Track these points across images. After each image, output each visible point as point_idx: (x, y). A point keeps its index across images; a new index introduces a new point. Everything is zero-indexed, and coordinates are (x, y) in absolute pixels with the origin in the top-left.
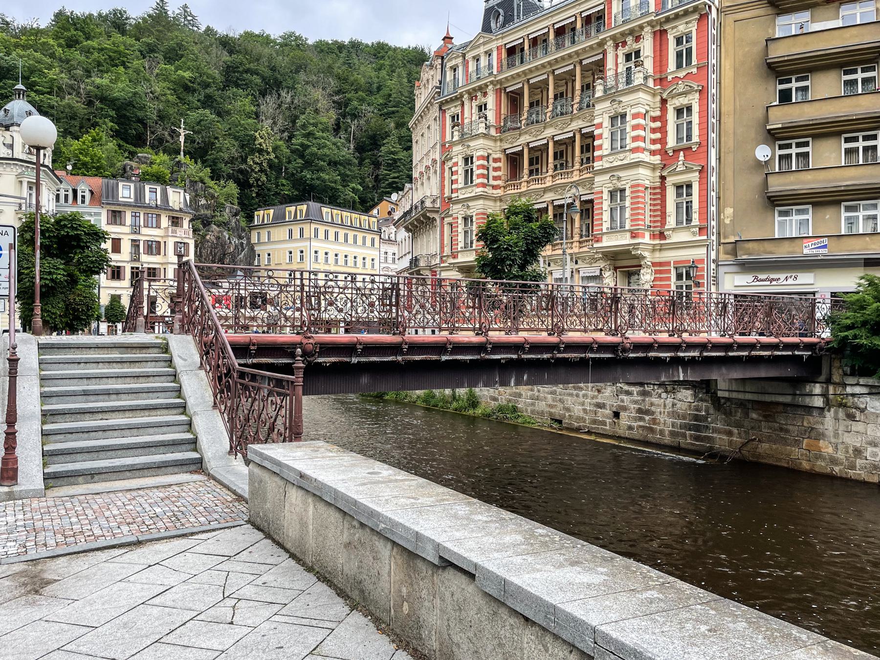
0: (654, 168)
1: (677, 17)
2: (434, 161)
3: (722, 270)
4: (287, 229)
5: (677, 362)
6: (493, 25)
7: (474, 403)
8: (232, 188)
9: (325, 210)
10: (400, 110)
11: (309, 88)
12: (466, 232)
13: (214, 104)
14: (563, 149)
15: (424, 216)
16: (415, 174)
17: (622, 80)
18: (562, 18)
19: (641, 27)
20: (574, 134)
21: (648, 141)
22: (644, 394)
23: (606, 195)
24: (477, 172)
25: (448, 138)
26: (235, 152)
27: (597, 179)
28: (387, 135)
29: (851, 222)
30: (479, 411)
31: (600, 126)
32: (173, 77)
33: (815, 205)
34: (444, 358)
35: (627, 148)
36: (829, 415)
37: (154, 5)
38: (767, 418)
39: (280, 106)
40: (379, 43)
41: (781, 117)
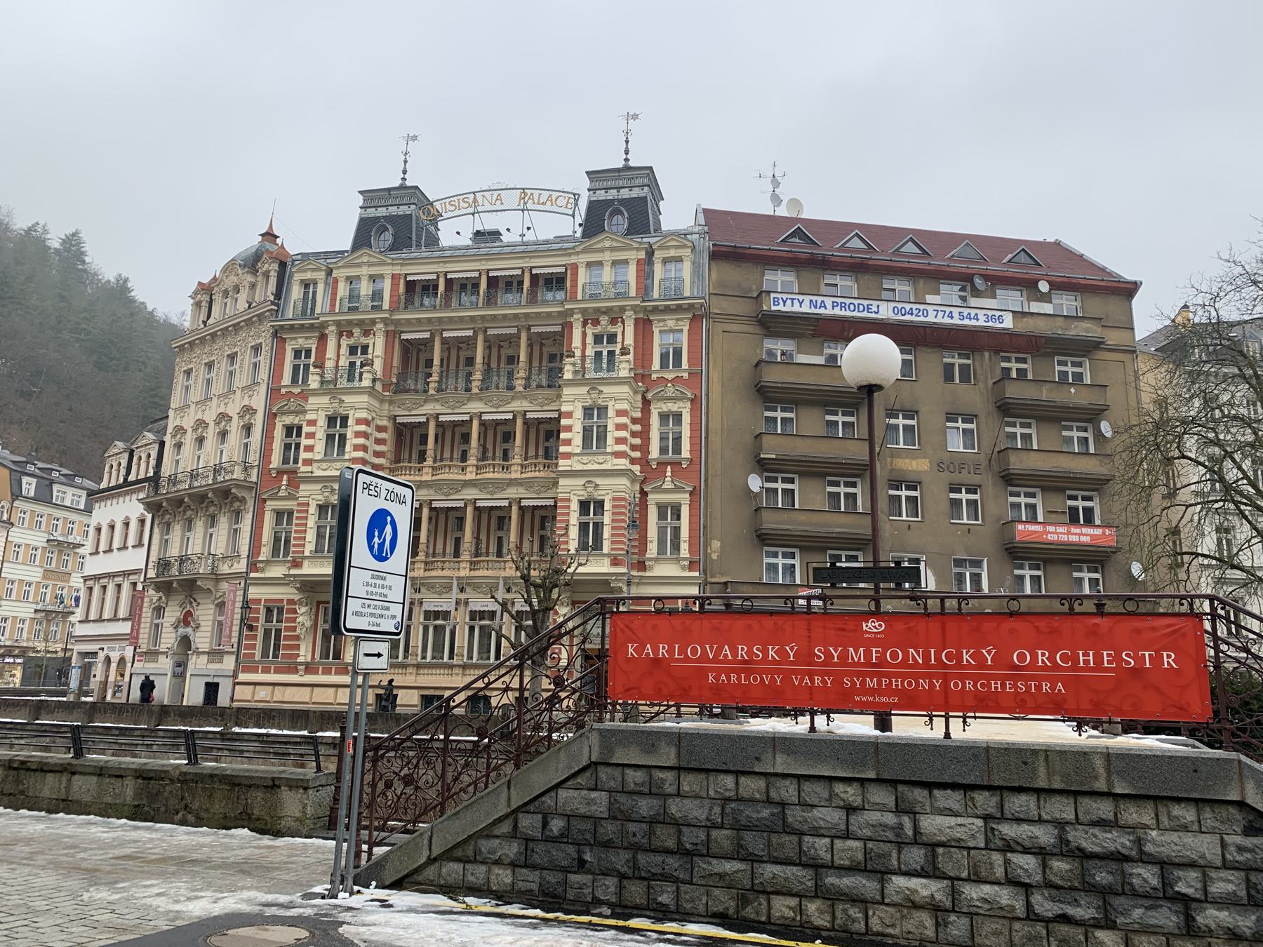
1: (667, 310)
14: (498, 434)
18: (460, 270)
19: (373, 322)
20: (515, 417)
21: (370, 451)
23: (575, 506)
24: (351, 441)
27: (562, 482)
35: (347, 457)
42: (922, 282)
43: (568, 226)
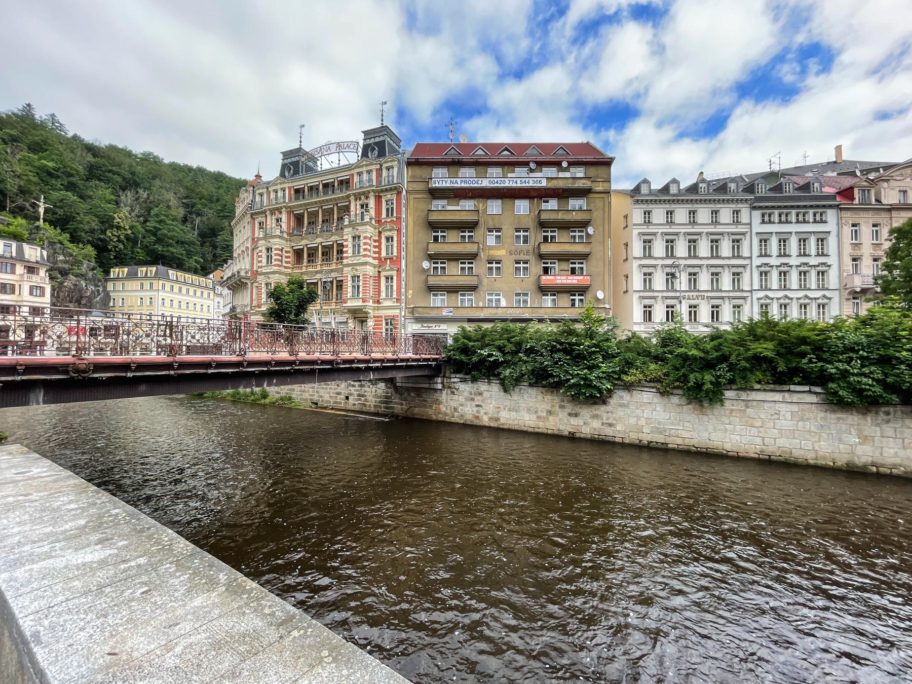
0: (375, 266)
1: (386, 190)
2: (247, 248)
3: (407, 321)
4: (139, 283)
5: (368, 369)
6: (287, 174)
7: (265, 395)
8: (90, 250)
9: (171, 272)
10: (227, 213)
11: (163, 191)
12: (354, 287)
13: (77, 189)
14: (327, 252)
15: (240, 281)
16: (235, 255)
17: (359, 218)
18: (328, 179)
19: (369, 192)
22: (361, 386)
23: (349, 278)
24: (274, 257)
25: (256, 235)
26: (95, 224)
28: (223, 229)
29: (462, 301)
30: (267, 401)
31: (346, 240)
32: (37, 164)
33: (448, 292)
34: (210, 371)
36: (444, 392)
37: (21, 108)
38: (418, 395)
39: (137, 199)
40: (219, 172)
41: (434, 248)
42: (506, 167)
43: (352, 158)
